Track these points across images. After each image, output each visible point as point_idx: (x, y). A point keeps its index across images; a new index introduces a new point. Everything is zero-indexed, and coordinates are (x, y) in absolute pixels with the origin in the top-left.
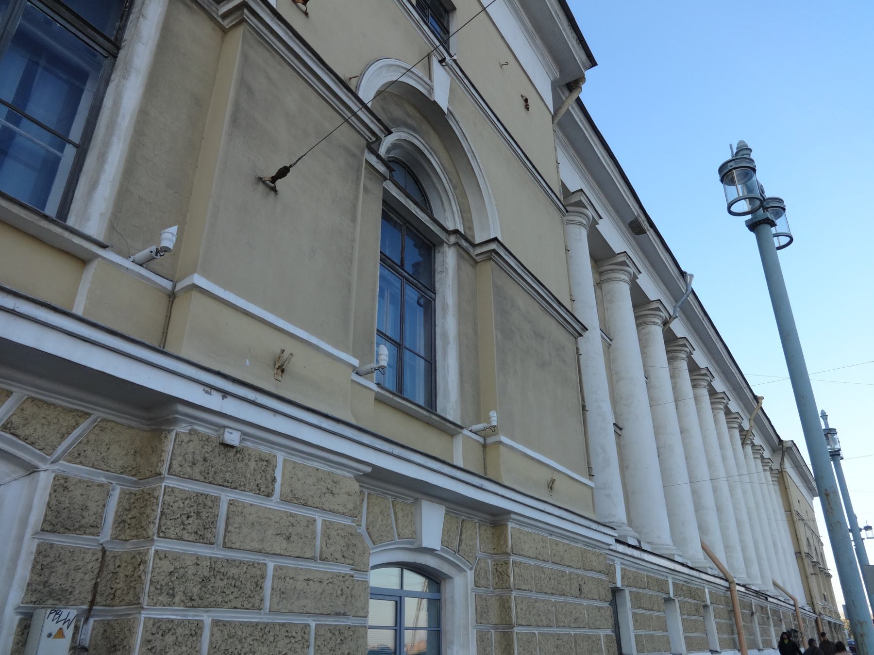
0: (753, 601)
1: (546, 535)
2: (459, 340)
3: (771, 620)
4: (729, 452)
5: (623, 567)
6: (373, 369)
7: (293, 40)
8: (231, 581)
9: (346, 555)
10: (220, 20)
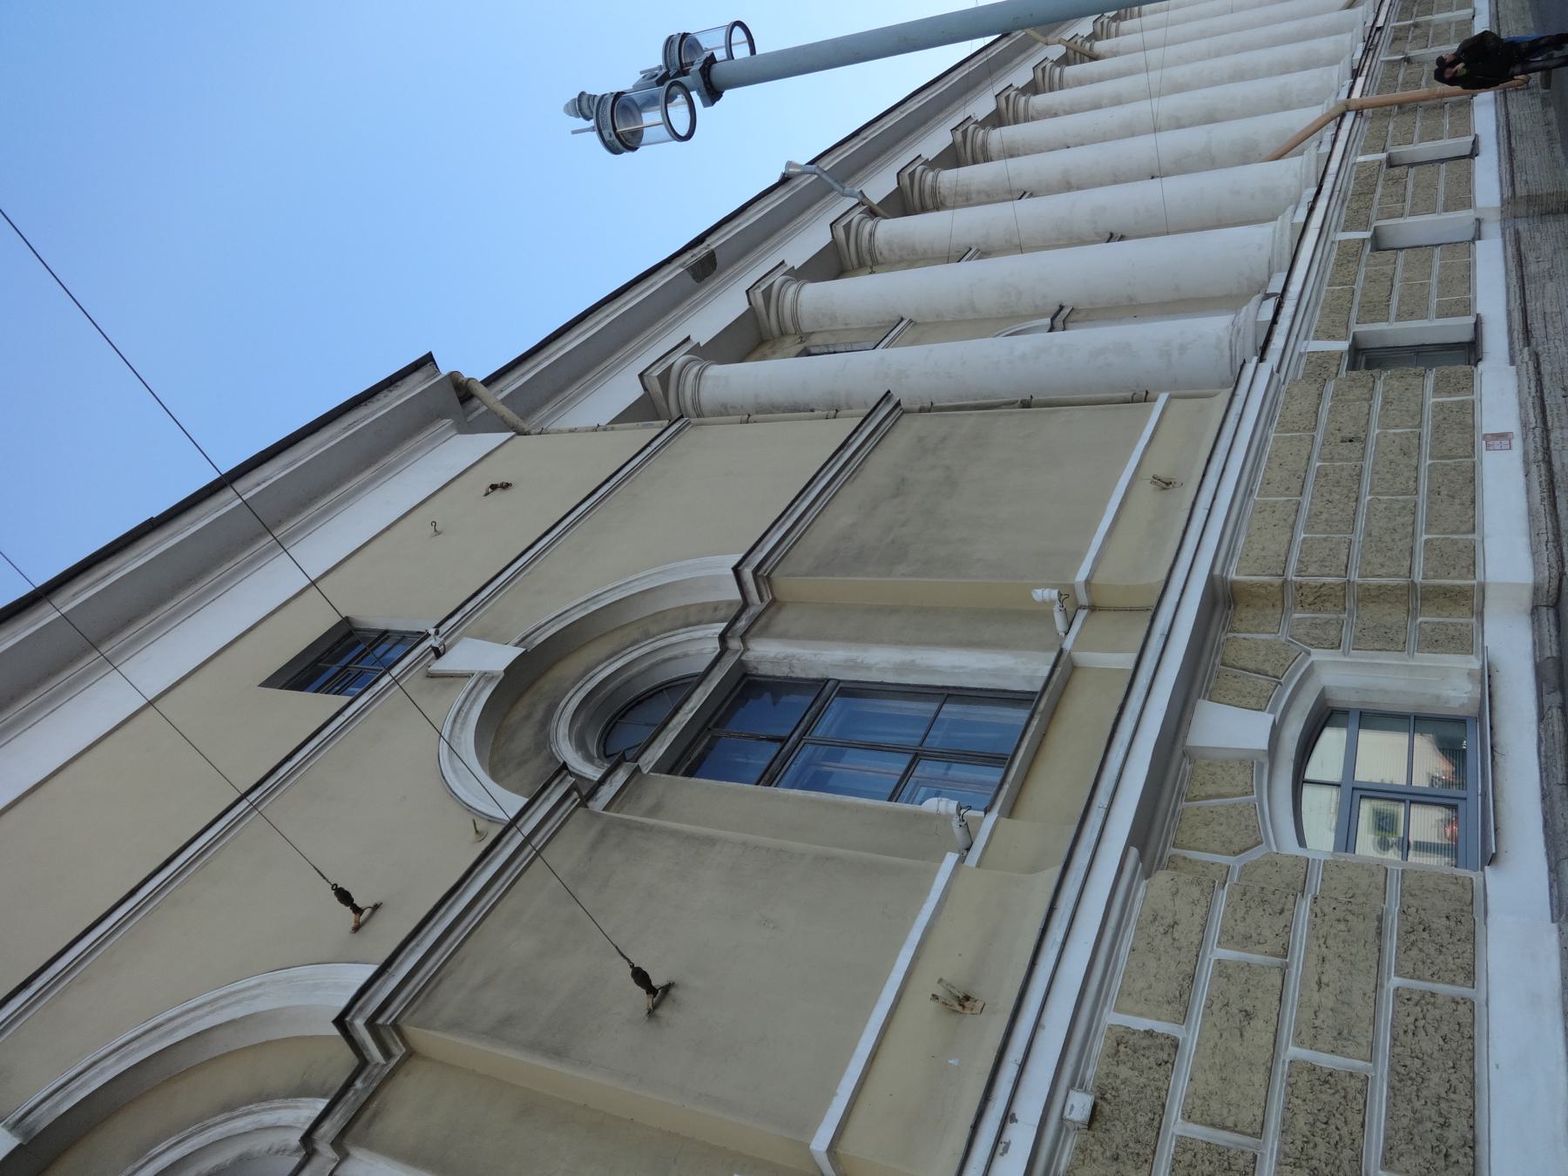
0: (1382, 58)
1: (1251, 503)
2: (908, 644)
3: (1419, 19)
4: (1107, 88)
5: (1312, 334)
6: (963, 824)
7: (422, 940)
8: (1317, 1130)
9: (1279, 907)
10: (393, 1062)
